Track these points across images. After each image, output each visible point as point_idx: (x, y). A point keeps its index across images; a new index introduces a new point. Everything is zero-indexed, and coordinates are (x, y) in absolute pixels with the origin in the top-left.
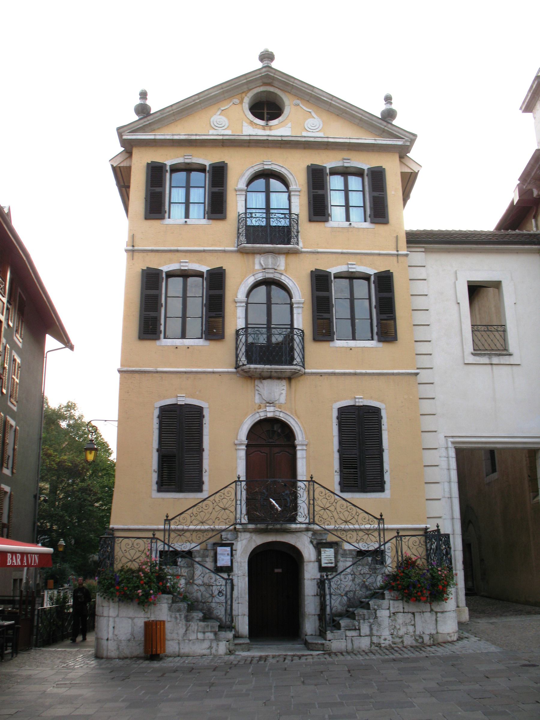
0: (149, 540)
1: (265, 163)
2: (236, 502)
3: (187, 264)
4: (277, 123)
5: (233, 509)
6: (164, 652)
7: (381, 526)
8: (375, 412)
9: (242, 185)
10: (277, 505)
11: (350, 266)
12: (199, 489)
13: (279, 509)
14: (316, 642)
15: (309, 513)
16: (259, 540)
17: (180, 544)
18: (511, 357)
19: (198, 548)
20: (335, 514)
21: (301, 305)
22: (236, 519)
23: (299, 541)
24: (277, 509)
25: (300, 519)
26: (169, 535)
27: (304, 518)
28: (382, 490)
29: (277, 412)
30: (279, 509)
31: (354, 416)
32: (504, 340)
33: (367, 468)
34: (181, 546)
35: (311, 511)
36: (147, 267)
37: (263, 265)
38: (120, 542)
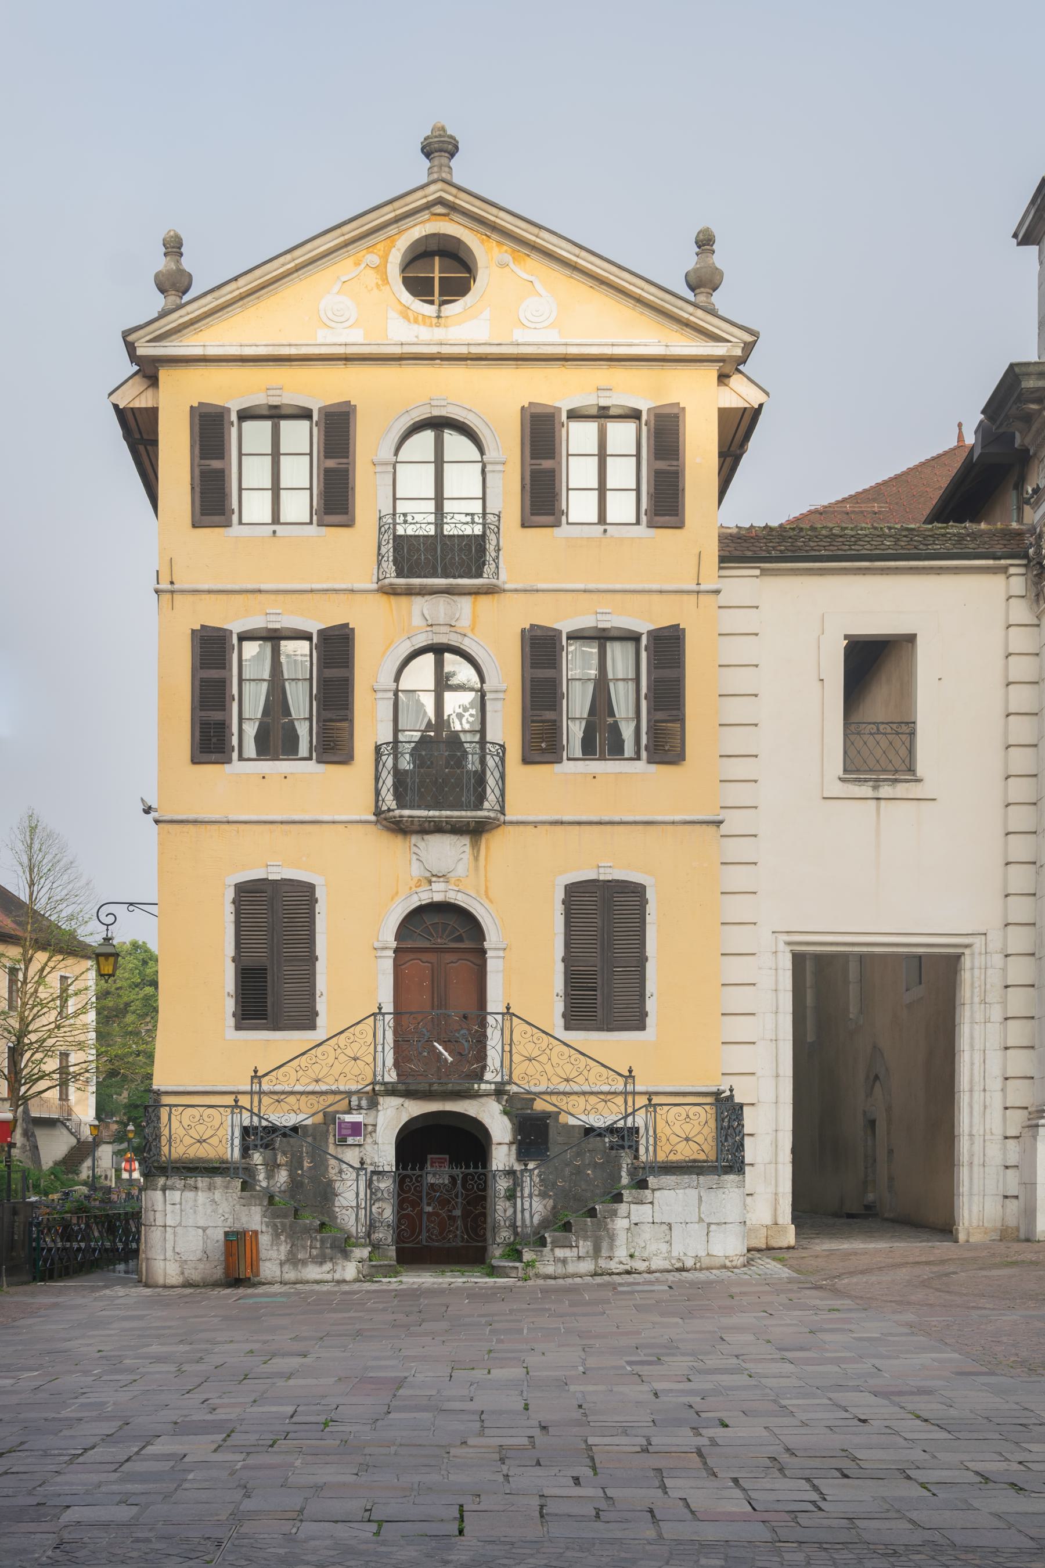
0: (229, 1110)
1: (434, 403)
2: (375, 1048)
3: (279, 618)
4: (461, 311)
5: (369, 1059)
6: (258, 1275)
7: (630, 1088)
8: (634, 893)
9: (386, 453)
10: (446, 1054)
11: (600, 617)
12: (312, 1027)
13: (450, 1059)
14: (506, 1264)
15: (502, 1066)
16: (416, 1108)
17: (278, 1115)
18: (919, 785)
19: (309, 1122)
20: (548, 1067)
21: (501, 695)
22: (375, 1075)
23: (484, 1111)
24: (446, 1059)
25: (488, 1076)
26: (260, 1102)
27: (495, 1073)
28: (642, 1027)
29: (451, 892)
30: (450, 1059)
31: (595, 899)
32: (910, 752)
33: (616, 990)
34: (283, 1117)
35: (507, 1062)
36: (202, 626)
37: (428, 617)
38: (180, 1112)
